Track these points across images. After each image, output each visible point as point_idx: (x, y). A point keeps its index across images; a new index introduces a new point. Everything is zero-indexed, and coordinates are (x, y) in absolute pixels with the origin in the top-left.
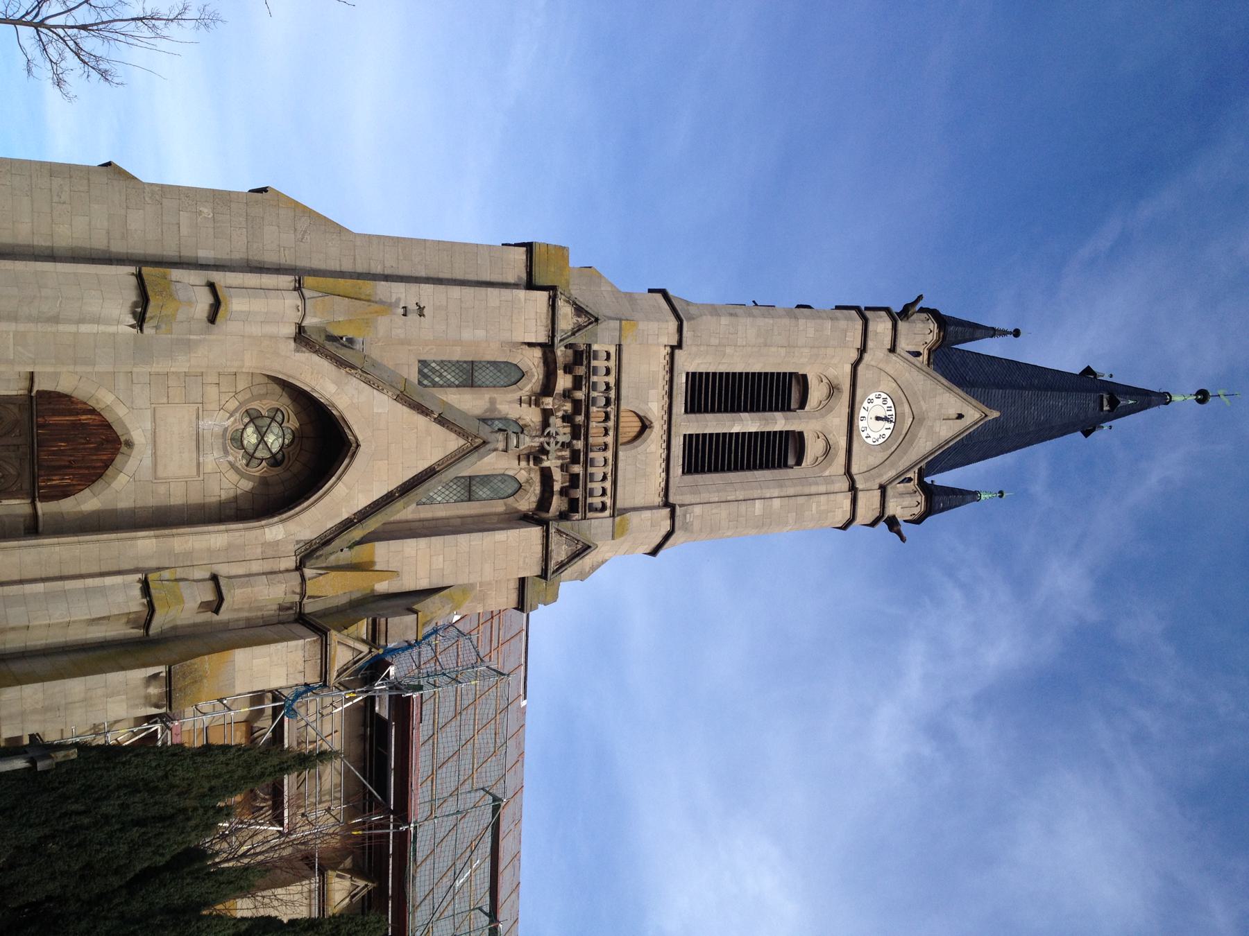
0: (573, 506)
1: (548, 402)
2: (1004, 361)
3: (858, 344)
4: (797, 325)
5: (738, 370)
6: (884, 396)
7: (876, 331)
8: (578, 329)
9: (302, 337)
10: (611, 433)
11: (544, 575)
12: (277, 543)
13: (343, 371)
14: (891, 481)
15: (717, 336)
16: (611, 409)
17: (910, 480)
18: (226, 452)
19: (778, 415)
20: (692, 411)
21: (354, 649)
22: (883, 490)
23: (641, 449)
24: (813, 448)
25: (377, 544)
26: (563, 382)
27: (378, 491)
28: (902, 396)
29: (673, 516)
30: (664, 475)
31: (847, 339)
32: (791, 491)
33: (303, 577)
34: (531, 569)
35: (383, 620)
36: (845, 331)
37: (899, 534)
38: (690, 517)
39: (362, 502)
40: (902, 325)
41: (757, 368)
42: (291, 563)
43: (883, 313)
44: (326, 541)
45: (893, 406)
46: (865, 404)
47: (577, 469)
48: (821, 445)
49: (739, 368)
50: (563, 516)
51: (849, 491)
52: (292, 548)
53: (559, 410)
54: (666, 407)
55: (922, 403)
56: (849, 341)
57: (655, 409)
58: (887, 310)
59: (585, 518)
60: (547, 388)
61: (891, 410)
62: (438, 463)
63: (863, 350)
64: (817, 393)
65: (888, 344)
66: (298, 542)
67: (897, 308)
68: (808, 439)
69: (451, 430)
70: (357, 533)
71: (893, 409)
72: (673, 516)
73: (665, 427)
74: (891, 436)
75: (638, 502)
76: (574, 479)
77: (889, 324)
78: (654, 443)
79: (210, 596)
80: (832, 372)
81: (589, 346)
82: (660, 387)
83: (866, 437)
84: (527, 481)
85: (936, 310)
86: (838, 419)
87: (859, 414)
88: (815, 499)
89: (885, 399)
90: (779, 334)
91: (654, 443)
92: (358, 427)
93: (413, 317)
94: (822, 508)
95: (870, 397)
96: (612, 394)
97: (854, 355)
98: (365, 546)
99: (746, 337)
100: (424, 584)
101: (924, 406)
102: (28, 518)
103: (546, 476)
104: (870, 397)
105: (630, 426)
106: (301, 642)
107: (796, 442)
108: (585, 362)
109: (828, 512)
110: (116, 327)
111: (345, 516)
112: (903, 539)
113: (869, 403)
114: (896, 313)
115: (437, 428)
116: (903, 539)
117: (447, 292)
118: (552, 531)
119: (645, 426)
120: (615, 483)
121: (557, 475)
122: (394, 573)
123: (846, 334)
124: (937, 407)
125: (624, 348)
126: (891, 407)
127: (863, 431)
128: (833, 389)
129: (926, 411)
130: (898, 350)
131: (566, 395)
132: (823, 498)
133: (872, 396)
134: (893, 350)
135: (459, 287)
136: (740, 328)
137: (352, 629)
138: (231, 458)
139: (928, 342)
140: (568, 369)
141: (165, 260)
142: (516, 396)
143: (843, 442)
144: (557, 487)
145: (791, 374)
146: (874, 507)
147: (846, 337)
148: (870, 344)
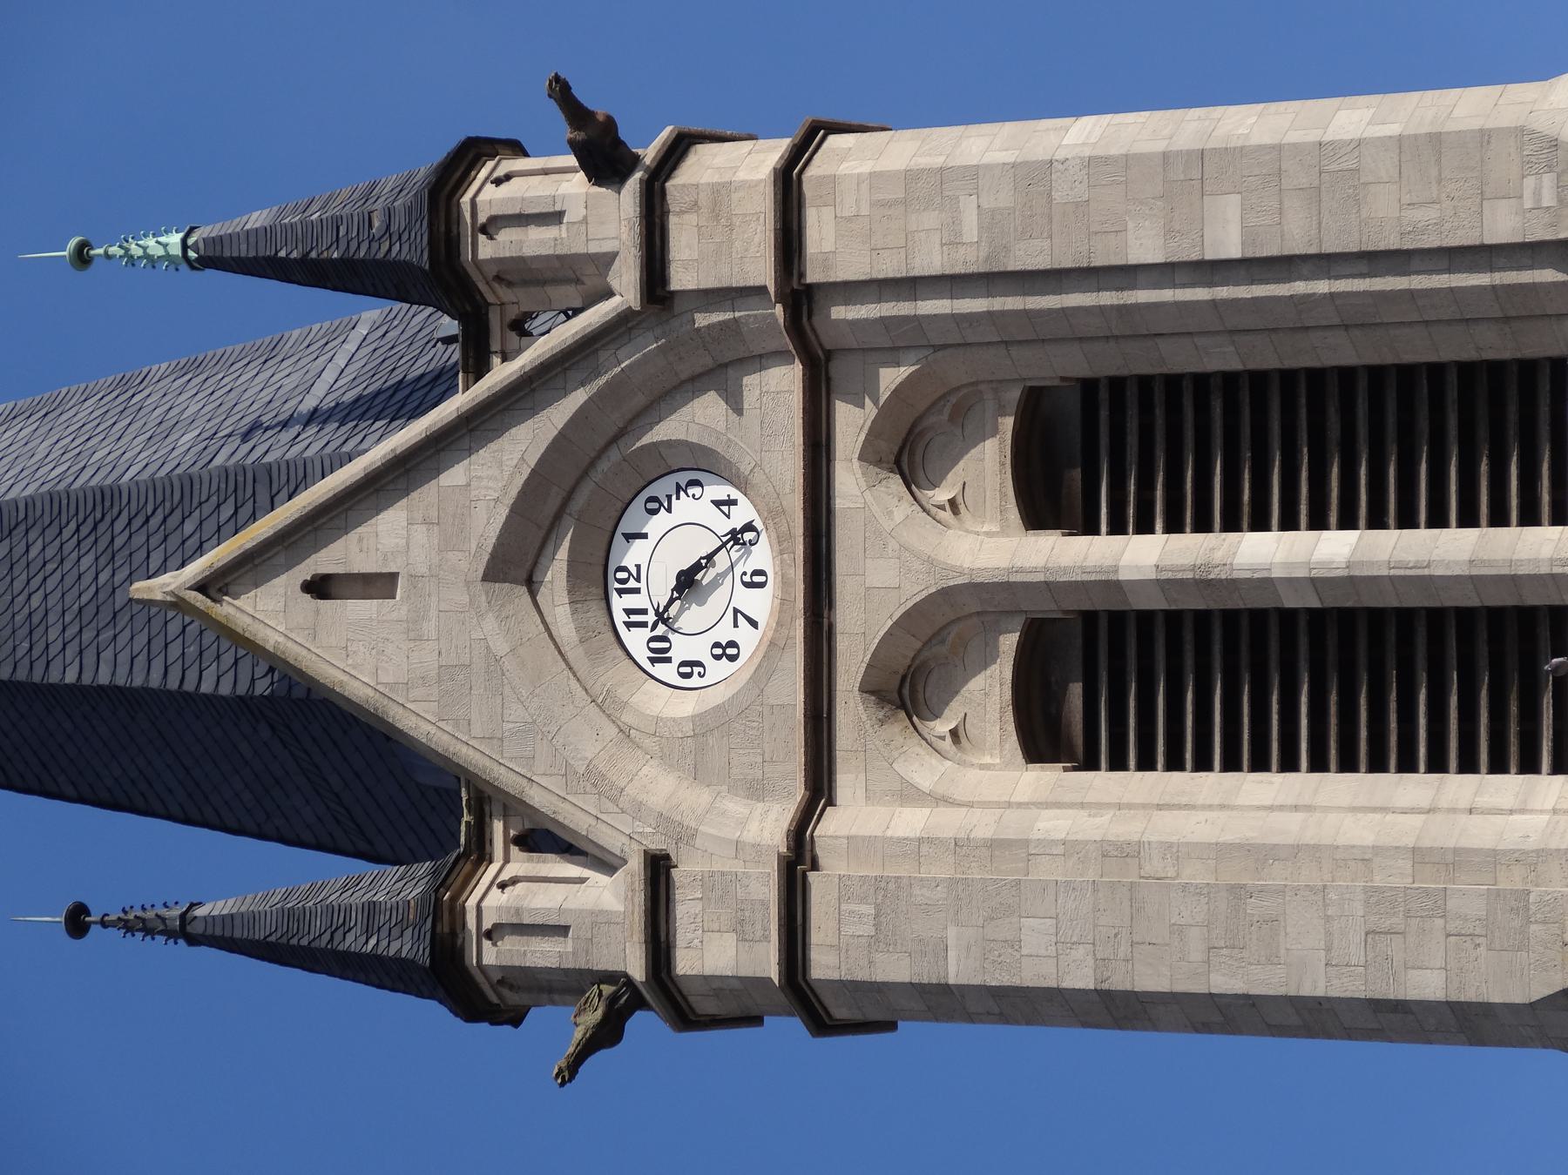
2: (70, 791)
4: (1101, 962)
7: (742, 939)
15: (1451, 928)
22: (659, 292)
31: (869, 910)
36: (879, 939)
37: (575, 112)
38: (1537, 193)
43: (840, 1012)
45: (622, 629)
46: (748, 639)
51: (810, 288)
55: (500, 646)
56: (863, 900)
58: (821, 1023)
61: (629, 612)
67: (645, 1026)
68: (1003, 495)
71: (620, 618)
74: (620, 505)
77: (686, 963)
83: (733, 502)
85: (467, 1020)
86: (874, 579)
87: (784, 602)
89: (660, 657)
90: (1179, 930)
94: (930, 219)
99: (1328, 919)
109: (905, 202)
110: (1440, 963)
112: (562, 92)
113: (732, 644)
114: (649, 1008)
116: (562, 92)
117: (733, 304)
123: (877, 926)
124: (430, 627)
126: (629, 625)
127: (749, 527)
129: (480, 616)
132: (931, 261)
135: (1129, 263)
136: (1357, 955)
139: (495, 891)
141: (833, 693)
145: (1090, 764)
146: (692, 219)
147: (877, 916)
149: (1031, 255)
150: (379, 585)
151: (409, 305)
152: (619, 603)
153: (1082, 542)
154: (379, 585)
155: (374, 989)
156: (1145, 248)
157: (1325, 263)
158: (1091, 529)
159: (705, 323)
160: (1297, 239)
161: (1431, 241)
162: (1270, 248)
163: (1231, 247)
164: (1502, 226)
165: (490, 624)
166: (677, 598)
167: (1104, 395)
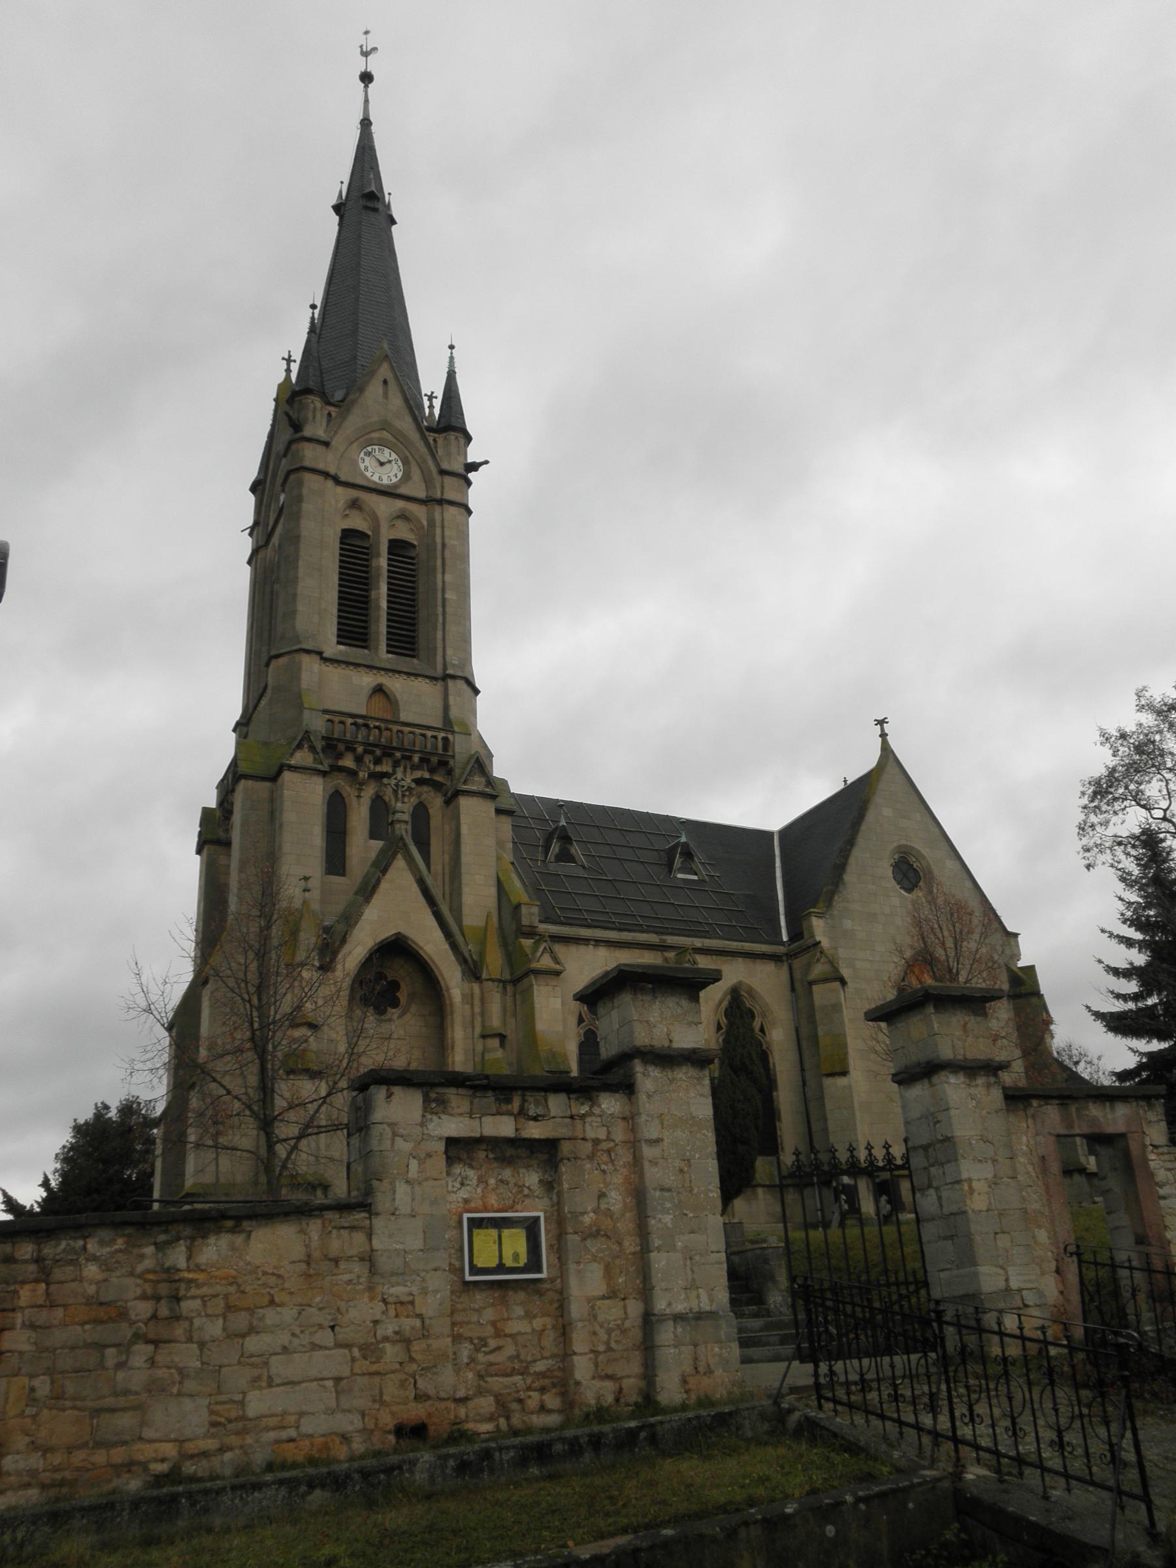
0: (443, 763)
1: (363, 775)
3: (320, 478)
5: (335, 595)
6: (362, 455)
8: (312, 749)
9: (326, 967)
10: (390, 726)
11: (493, 797)
12: (463, 995)
13: (349, 940)
14: (438, 465)
16: (372, 724)
17: (435, 440)
18: (390, 1020)
19: (374, 563)
20: (365, 641)
21: (543, 953)
23: (399, 698)
24: (404, 532)
25: (464, 923)
26: (348, 762)
27: (431, 922)
28: (365, 438)
29: (454, 677)
30: (420, 679)
32: (439, 562)
33: (487, 980)
34: (489, 807)
35: (524, 928)
39: (438, 934)
40: (308, 432)
41: (335, 579)
42: (476, 987)
44: (462, 959)
46: (368, 474)
47: (416, 758)
48: (400, 524)
49: (334, 595)
50: (450, 772)
52: (466, 984)
53: (369, 768)
54: (367, 670)
57: (367, 680)
59: (453, 757)
60: (352, 773)
62: (415, 876)
63: (326, 474)
64: (358, 522)
65: (320, 449)
66: (463, 980)
69: (391, 864)
70: (459, 938)
71: (374, 447)
72: (454, 677)
73: (383, 673)
75: (439, 704)
76: (424, 760)
78: (396, 685)
79: (495, 1042)
80: (341, 504)
81: (323, 738)
82: (351, 673)
84: (419, 797)
88: (447, 540)
91: (396, 685)
92: (387, 933)
93: (310, 884)
95: (363, 468)
96: (360, 721)
97: (330, 484)
98: (466, 933)
100: (493, 891)
101: (375, 419)
102: (909, 990)
103: (419, 782)
104: (363, 468)
105: (379, 705)
106: (535, 987)
107: (398, 547)
108: (335, 742)
111: (447, 947)
115: (388, 875)
116: (486, 462)
118: (465, 787)
119: (379, 690)
120: (429, 728)
121: (418, 774)
122: (488, 916)
125: (326, 707)
128: (355, 504)
130: (327, 439)
131: (359, 760)
132: (447, 533)
133: (362, 466)
134: (327, 444)
137: (528, 951)
138: (395, 1017)
140: (340, 756)
142: (354, 800)
143: (400, 504)
144: (427, 775)
145: (341, 543)
148: (321, 466)
149: (447, 554)
150: (386, 395)
151: (786, 1363)
152: (376, 447)
153: (386, 550)
154: (386, 395)
155: (1003, 919)
156: (448, 578)
157: (444, 613)
158: (389, 553)
159: (1159, 1087)
160: (448, 609)
161: (447, 637)
162: (447, 604)
163: (447, 596)
164: (449, 652)
165: (376, 419)
166: (1164, 893)
167: (365, 599)
